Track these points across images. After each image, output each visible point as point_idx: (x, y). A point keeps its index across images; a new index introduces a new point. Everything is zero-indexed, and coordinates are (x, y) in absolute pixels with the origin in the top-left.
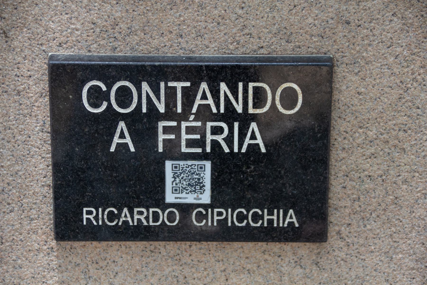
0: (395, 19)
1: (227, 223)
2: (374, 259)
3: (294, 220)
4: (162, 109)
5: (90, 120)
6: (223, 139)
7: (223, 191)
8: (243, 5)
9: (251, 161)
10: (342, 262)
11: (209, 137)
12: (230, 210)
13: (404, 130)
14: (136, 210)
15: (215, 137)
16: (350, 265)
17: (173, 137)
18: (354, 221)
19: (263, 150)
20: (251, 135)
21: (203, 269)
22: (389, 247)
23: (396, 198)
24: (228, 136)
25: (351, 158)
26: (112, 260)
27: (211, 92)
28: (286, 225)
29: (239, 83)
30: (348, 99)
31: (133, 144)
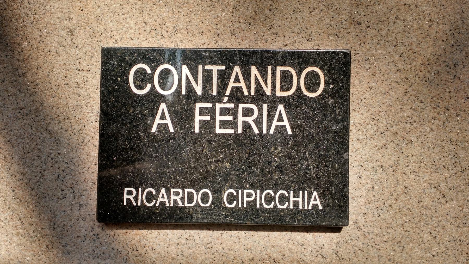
0: (398, 21)
1: (256, 205)
2: (388, 249)
3: (318, 202)
4: (199, 91)
5: (135, 102)
6: (253, 121)
7: (252, 172)
8: (271, 7)
9: (278, 142)
10: (359, 251)
11: (241, 119)
12: (258, 191)
13: (410, 123)
14: (173, 190)
15: (246, 119)
16: (366, 255)
17: (208, 118)
18: (370, 210)
19: (290, 132)
20: (279, 117)
21: (232, 257)
22: (401, 237)
23: (406, 188)
24: (258, 117)
25: (365, 148)
26: (150, 248)
27: (243, 75)
28: (310, 208)
29: (268, 67)
30: (361, 93)
31: (173, 124)
